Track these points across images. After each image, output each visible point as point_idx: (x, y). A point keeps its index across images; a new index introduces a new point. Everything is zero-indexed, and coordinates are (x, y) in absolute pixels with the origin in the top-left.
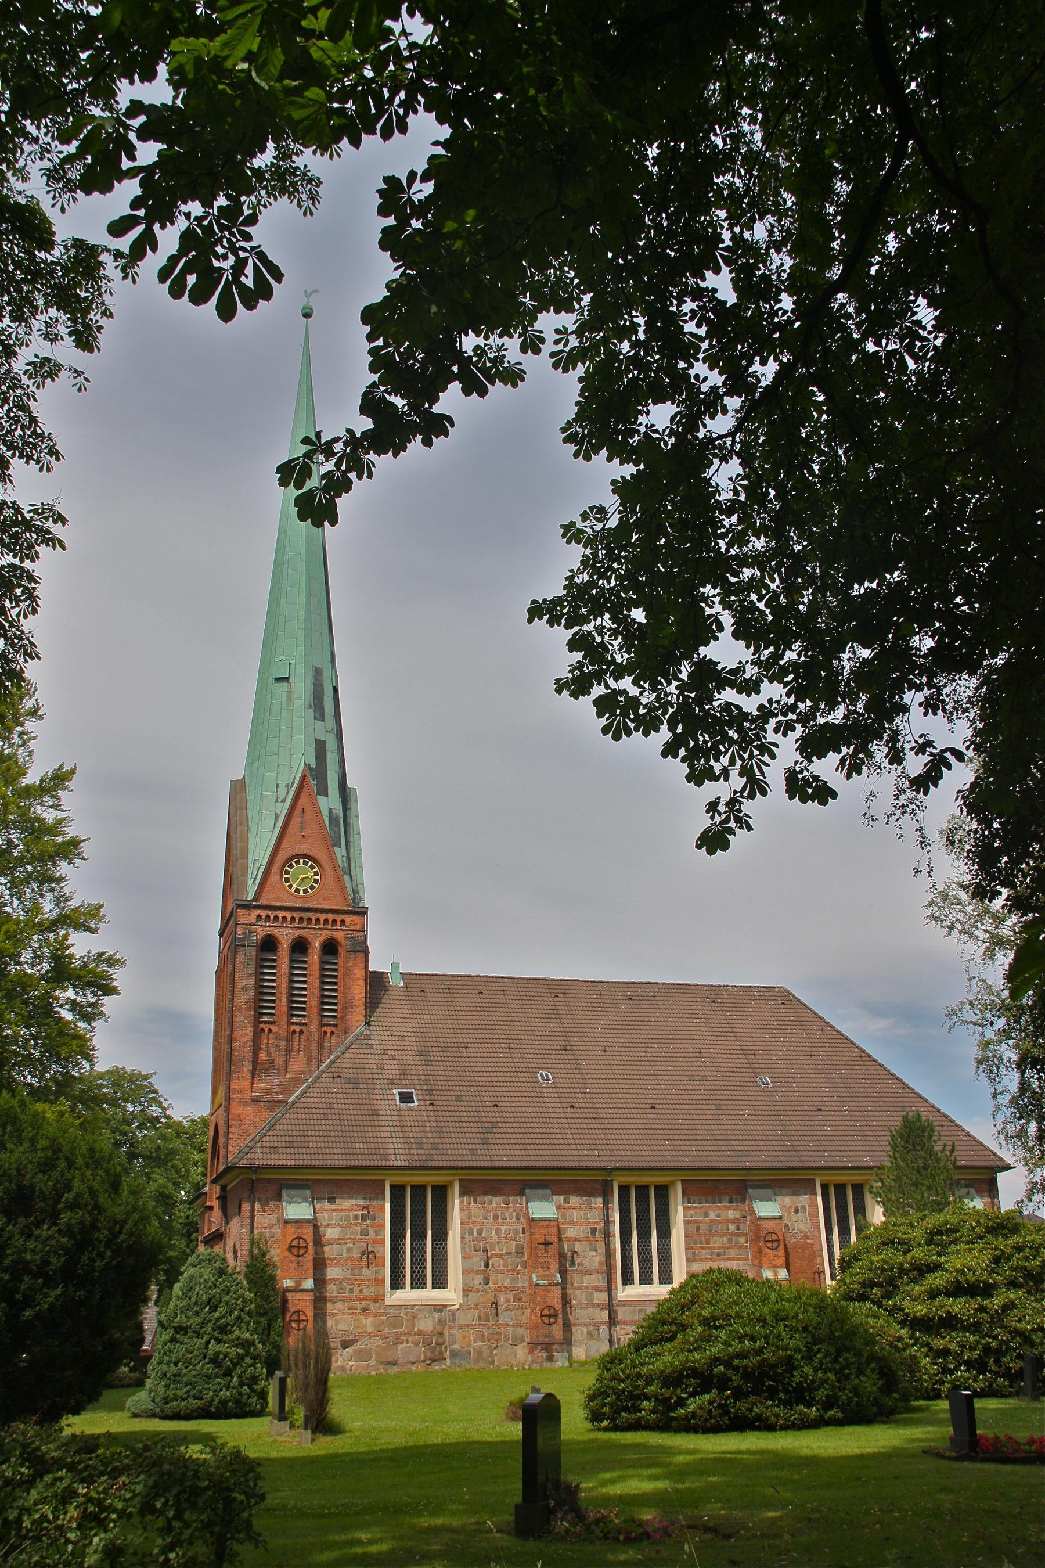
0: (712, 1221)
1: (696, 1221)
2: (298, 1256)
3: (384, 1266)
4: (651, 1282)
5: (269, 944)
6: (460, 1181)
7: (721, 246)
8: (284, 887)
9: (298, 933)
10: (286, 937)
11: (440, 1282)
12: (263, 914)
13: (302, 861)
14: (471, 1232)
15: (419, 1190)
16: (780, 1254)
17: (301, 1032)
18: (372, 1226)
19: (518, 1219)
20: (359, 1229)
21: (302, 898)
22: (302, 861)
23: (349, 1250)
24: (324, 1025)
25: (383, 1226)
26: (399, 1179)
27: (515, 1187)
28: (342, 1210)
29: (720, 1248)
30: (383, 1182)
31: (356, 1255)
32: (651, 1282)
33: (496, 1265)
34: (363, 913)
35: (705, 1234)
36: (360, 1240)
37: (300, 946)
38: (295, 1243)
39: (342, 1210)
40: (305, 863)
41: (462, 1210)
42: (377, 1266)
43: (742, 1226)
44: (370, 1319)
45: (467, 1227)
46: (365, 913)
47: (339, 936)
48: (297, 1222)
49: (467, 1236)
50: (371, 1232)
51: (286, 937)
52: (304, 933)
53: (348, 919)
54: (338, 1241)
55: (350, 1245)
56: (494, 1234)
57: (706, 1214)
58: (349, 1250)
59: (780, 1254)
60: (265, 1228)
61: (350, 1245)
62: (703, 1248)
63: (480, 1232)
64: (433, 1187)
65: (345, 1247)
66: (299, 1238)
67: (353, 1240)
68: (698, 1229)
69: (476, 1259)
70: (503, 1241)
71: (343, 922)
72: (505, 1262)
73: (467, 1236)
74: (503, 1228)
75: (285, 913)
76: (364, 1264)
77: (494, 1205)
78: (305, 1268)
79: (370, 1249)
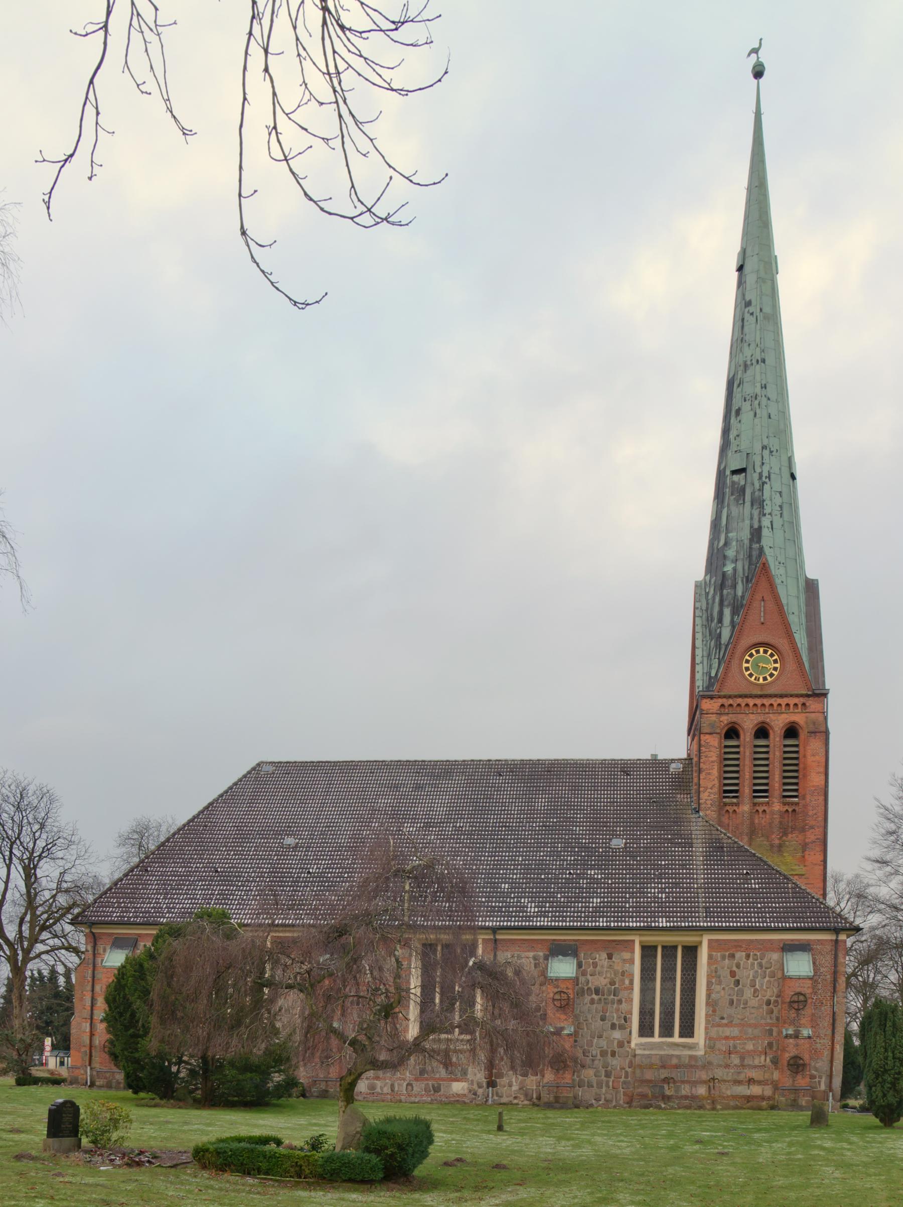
4: (652, 1035)
5: (732, 733)
8: (744, 675)
9: (760, 718)
10: (748, 723)
11: (688, 1030)
12: (727, 702)
13: (761, 650)
15: (669, 951)
17: (794, 811)
21: (762, 685)
22: (761, 650)
24: (725, 804)
26: (651, 939)
30: (633, 941)
32: (652, 1035)
34: (823, 695)
37: (762, 732)
40: (765, 652)
46: (825, 695)
51: (748, 723)
53: (810, 702)
64: (664, 947)
71: (804, 704)
75: (779, 701)
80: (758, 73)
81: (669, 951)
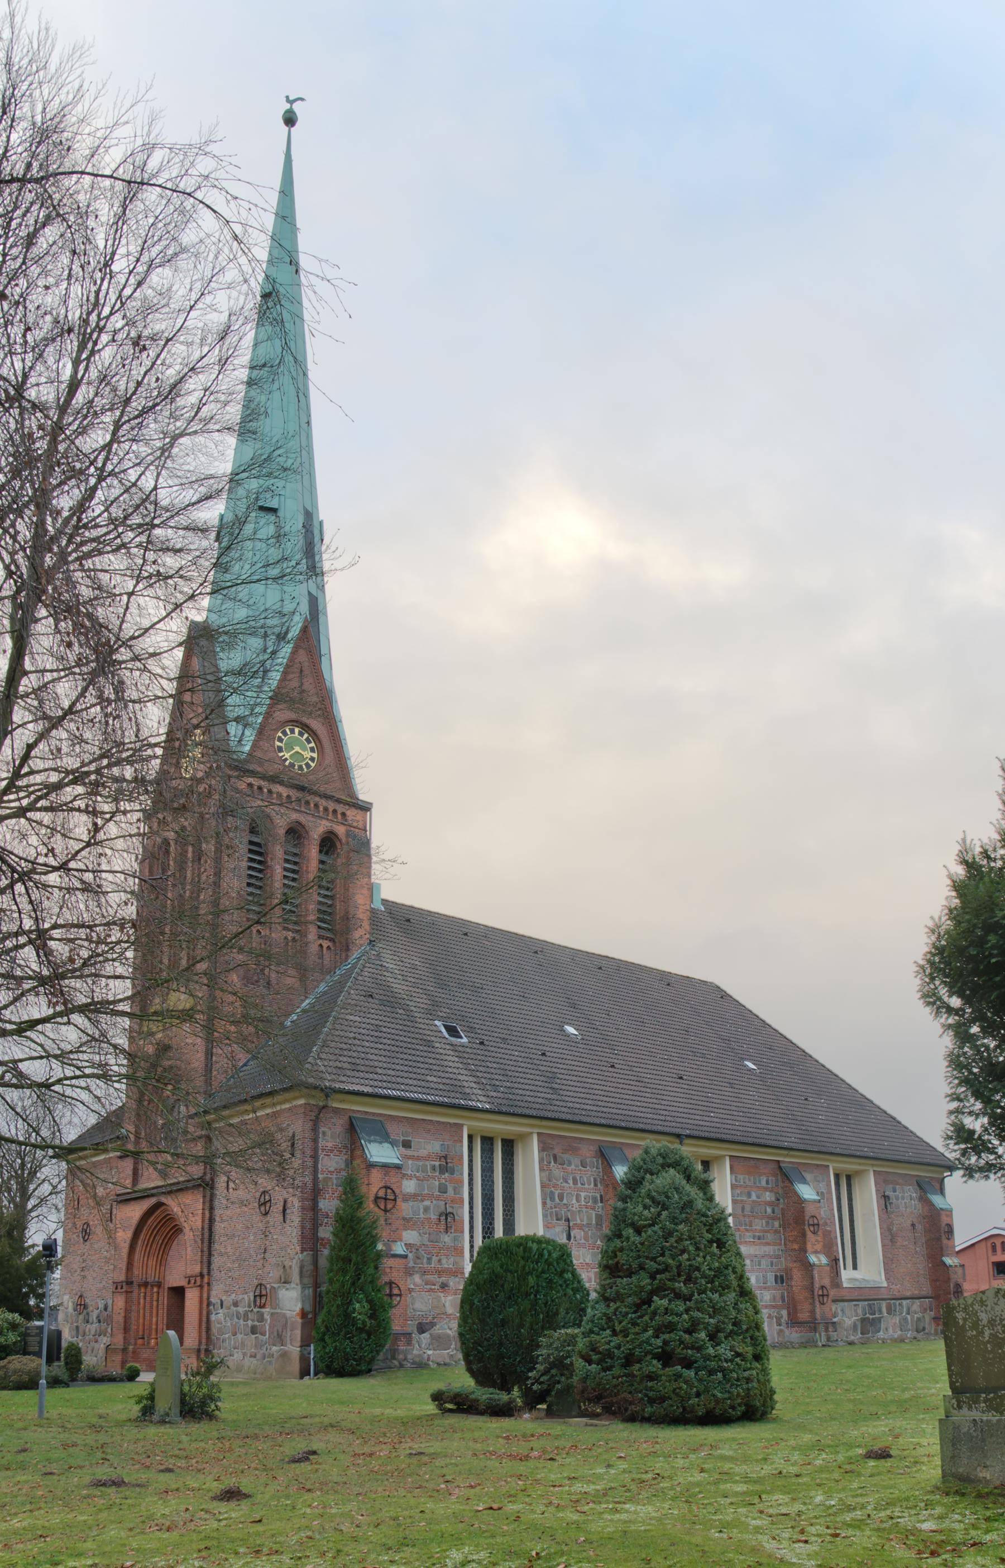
0: (753, 1201)
1: (742, 1201)
2: (386, 1211)
3: (462, 1232)
6: (539, 1134)
7: (70, 559)
9: (295, 816)
14: (552, 1199)
16: (819, 1238)
18: (451, 1182)
19: (596, 1185)
20: (437, 1183)
23: (426, 1209)
25: (462, 1182)
27: (592, 1148)
28: (418, 1158)
29: (760, 1231)
30: (462, 1125)
31: (433, 1216)
33: (578, 1237)
35: (749, 1216)
36: (438, 1198)
38: (381, 1194)
39: (418, 1158)
41: (541, 1169)
42: (456, 1231)
43: (776, 1209)
44: (450, 1298)
45: (548, 1190)
47: (341, 830)
48: (385, 1166)
49: (548, 1201)
50: (450, 1189)
52: (302, 818)
54: (414, 1197)
55: (427, 1203)
56: (574, 1201)
57: (749, 1195)
58: (426, 1209)
59: (819, 1238)
60: (331, 1173)
61: (427, 1203)
62: (747, 1230)
63: (561, 1199)
65: (421, 1205)
66: (387, 1187)
67: (431, 1197)
68: (743, 1209)
69: (558, 1229)
70: (584, 1210)
72: (586, 1233)
73: (548, 1201)
74: (583, 1194)
76: (443, 1227)
77: (573, 1167)
78: (393, 1228)
79: (449, 1210)
80: (290, 120)
81: (488, 1141)
